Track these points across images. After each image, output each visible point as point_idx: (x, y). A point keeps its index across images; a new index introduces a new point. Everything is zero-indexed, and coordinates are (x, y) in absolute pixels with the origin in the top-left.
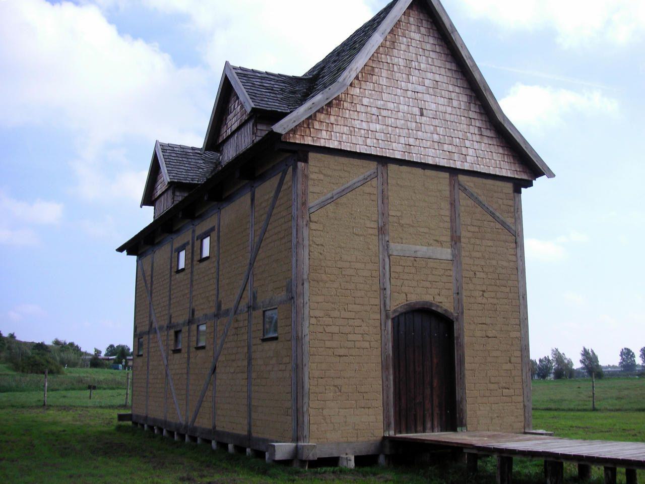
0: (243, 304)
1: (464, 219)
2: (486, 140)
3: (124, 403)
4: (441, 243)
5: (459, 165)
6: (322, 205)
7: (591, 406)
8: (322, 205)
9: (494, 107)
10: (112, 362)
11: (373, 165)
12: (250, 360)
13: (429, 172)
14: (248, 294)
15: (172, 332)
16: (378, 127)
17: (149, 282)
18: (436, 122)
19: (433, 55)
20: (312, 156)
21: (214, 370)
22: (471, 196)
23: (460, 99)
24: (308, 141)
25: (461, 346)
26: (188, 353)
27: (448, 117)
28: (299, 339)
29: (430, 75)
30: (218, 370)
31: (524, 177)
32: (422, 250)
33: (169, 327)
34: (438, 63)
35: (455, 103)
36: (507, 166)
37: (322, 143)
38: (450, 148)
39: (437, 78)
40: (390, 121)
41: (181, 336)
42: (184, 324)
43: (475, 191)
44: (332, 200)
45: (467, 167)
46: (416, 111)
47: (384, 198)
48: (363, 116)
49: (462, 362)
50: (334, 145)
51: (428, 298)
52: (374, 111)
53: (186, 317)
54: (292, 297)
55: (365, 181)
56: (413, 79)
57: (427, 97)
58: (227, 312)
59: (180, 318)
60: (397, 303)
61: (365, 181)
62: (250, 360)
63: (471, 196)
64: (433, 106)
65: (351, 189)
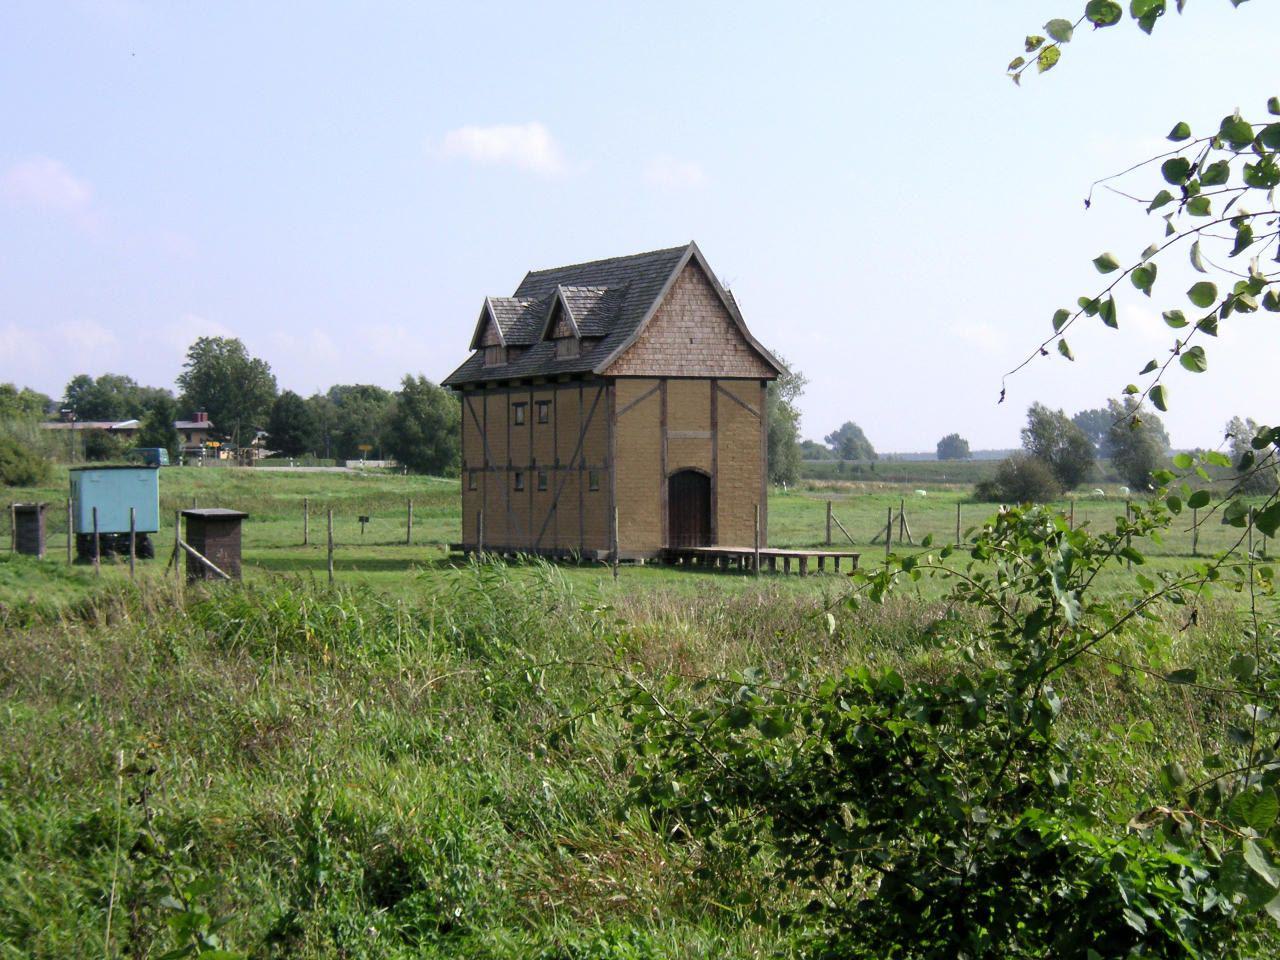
0: (575, 465)
1: (721, 409)
2: (740, 354)
3: (405, 538)
4: (704, 429)
5: (717, 374)
6: (625, 410)
7: (1192, 552)
8: (625, 410)
9: (744, 332)
10: (133, 441)
11: (657, 382)
12: (581, 501)
13: (695, 381)
14: (578, 458)
15: (513, 474)
16: (660, 356)
17: (482, 425)
18: (701, 347)
19: (702, 298)
20: (618, 381)
21: (555, 506)
22: (727, 393)
23: (720, 326)
24: (616, 373)
25: (715, 493)
26: (531, 492)
27: (711, 341)
28: (610, 492)
29: (698, 313)
30: (559, 506)
31: (769, 375)
32: (690, 433)
33: (510, 468)
34: (705, 302)
35: (716, 330)
36: (754, 369)
37: (624, 373)
38: (712, 363)
39: (704, 314)
40: (668, 351)
41: (522, 478)
42: (526, 469)
43: (729, 390)
44: (630, 407)
45: (723, 374)
46: (688, 341)
47: (664, 403)
48: (650, 351)
49: (716, 503)
50: (631, 373)
51: (693, 464)
52: (658, 346)
53: (527, 464)
54: (608, 465)
55: (651, 393)
56: (686, 318)
57: (696, 330)
58: (564, 467)
59: (522, 462)
60: (672, 467)
61: (651, 393)
62: (581, 501)
63: (727, 393)
64: (700, 335)
65: (643, 398)
